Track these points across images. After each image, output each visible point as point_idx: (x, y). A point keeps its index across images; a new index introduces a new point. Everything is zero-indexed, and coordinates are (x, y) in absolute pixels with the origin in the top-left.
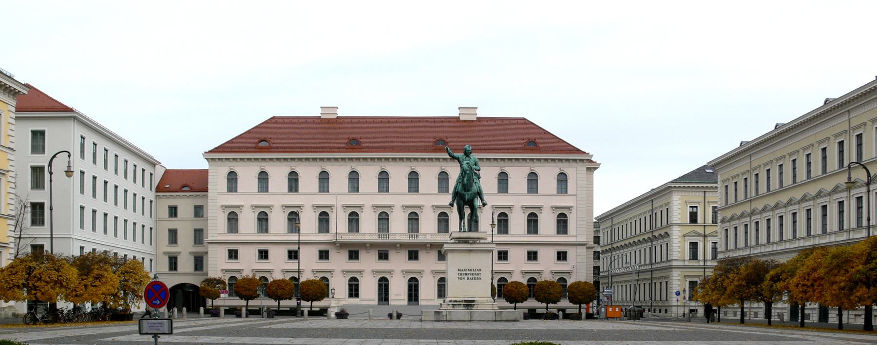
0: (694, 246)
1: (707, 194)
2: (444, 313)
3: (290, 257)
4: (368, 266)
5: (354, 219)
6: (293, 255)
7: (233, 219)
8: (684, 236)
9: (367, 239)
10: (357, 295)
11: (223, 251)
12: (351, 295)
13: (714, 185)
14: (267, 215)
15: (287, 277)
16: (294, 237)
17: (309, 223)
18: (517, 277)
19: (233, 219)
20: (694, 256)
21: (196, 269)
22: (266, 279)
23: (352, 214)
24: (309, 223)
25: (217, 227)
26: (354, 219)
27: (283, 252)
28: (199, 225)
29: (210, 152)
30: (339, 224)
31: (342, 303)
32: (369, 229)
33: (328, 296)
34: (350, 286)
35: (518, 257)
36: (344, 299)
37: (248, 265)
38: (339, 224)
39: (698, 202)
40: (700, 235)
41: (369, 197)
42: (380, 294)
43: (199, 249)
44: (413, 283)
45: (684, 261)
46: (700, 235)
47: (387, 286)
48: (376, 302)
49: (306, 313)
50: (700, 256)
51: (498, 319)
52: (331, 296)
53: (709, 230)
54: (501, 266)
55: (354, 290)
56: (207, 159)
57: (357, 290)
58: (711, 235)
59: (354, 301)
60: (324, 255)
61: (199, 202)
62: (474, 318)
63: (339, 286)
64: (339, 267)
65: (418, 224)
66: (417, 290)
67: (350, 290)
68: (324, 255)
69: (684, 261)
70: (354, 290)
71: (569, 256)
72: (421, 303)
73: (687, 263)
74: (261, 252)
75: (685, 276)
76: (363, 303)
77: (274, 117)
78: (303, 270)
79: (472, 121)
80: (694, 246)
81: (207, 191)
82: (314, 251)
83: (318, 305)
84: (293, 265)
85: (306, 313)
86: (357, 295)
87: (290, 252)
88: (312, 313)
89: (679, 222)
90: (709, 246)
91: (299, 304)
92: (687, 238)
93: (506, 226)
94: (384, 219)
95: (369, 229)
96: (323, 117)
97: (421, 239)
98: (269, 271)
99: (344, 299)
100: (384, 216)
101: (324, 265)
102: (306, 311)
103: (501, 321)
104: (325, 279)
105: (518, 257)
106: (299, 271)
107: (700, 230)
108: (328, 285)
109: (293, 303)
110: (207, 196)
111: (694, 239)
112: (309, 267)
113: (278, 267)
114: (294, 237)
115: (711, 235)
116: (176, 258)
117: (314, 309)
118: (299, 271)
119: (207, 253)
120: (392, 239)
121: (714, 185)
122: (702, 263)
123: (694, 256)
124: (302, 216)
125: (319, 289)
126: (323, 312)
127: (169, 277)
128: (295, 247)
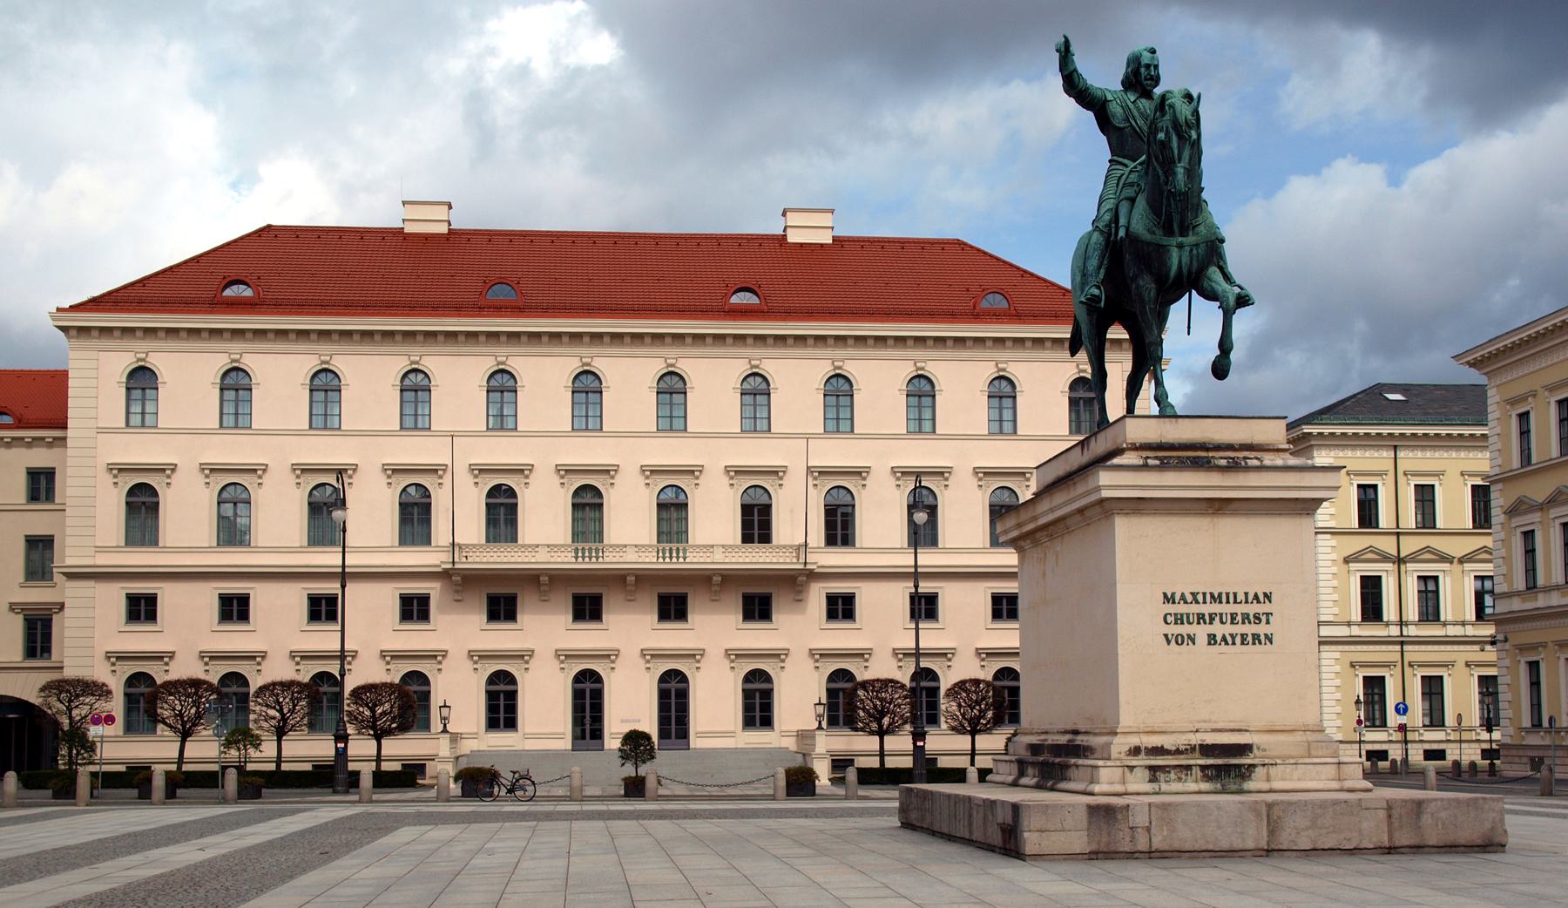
0: (1371, 588)
1: (1401, 454)
2: (1140, 819)
3: (314, 616)
4: (545, 639)
5: (502, 511)
6: (323, 609)
7: (142, 505)
8: (1347, 561)
9: (541, 560)
10: (511, 724)
11: (114, 597)
12: (492, 724)
13: (1478, 431)
14: (598, 493)
15: (306, 674)
16: (328, 558)
17: (371, 519)
18: (882, 667)
19: (142, 505)
20: (1372, 609)
21: (31, 652)
22: (237, 679)
23: (136, 490)
24: (371, 519)
25: (91, 525)
26: (502, 511)
27: (295, 597)
28: (39, 523)
29: (74, 308)
30: (460, 518)
31: (467, 746)
32: (545, 530)
33: (426, 726)
34: (492, 696)
35: (882, 610)
36: (475, 736)
37: (187, 638)
38: (460, 518)
39: (1379, 474)
40: (1385, 558)
41: (630, 445)
42: (578, 720)
43: (38, 595)
44: (673, 686)
45: (1463, 624)
46: (1385, 558)
47: (598, 695)
48: (566, 743)
49: (366, 781)
50: (1389, 611)
51: (1404, 839)
52: (436, 725)
53: (1410, 545)
54: (841, 637)
55: (502, 707)
56: (64, 329)
57: (512, 709)
58: (1413, 558)
59: (502, 740)
60: (414, 609)
61: (40, 458)
62: (1284, 840)
63: (459, 695)
64: (459, 641)
65: (601, 520)
66: (683, 709)
67: (492, 708)
68: (414, 609)
69: (1349, 624)
70: (502, 707)
71: (943, 606)
72: (695, 742)
73: (1356, 631)
74: (226, 600)
75: (1352, 665)
76: (531, 745)
77: (269, 226)
78: (355, 654)
79: (822, 245)
80: (1371, 588)
81: (63, 426)
82: (387, 597)
83: (400, 748)
84: (324, 638)
85: (366, 781)
86: (511, 724)
87: (314, 601)
88: (384, 780)
89: (1332, 524)
90: (1412, 588)
91: (341, 755)
92: (1467, 566)
93: (512, 521)
94: (588, 505)
95: (545, 530)
96: (410, 228)
97: (695, 560)
98: (250, 657)
99: (475, 736)
100: (588, 498)
101: (415, 638)
102: (367, 769)
103: (1418, 849)
104: (421, 678)
105: (882, 610)
106: (342, 656)
107: (1387, 545)
108: (426, 696)
109: (321, 748)
110: (65, 439)
111: (1372, 569)
112: (372, 641)
113: (279, 641)
114: (328, 558)
115: (1413, 558)
116: (47, 623)
117: (385, 766)
118: (342, 656)
119: (62, 606)
120: (611, 560)
121: (1478, 431)
122: (1394, 631)
123: (1372, 609)
124: (258, 496)
125: (408, 702)
126: (409, 776)
127: (23, 675)
128: (332, 587)
